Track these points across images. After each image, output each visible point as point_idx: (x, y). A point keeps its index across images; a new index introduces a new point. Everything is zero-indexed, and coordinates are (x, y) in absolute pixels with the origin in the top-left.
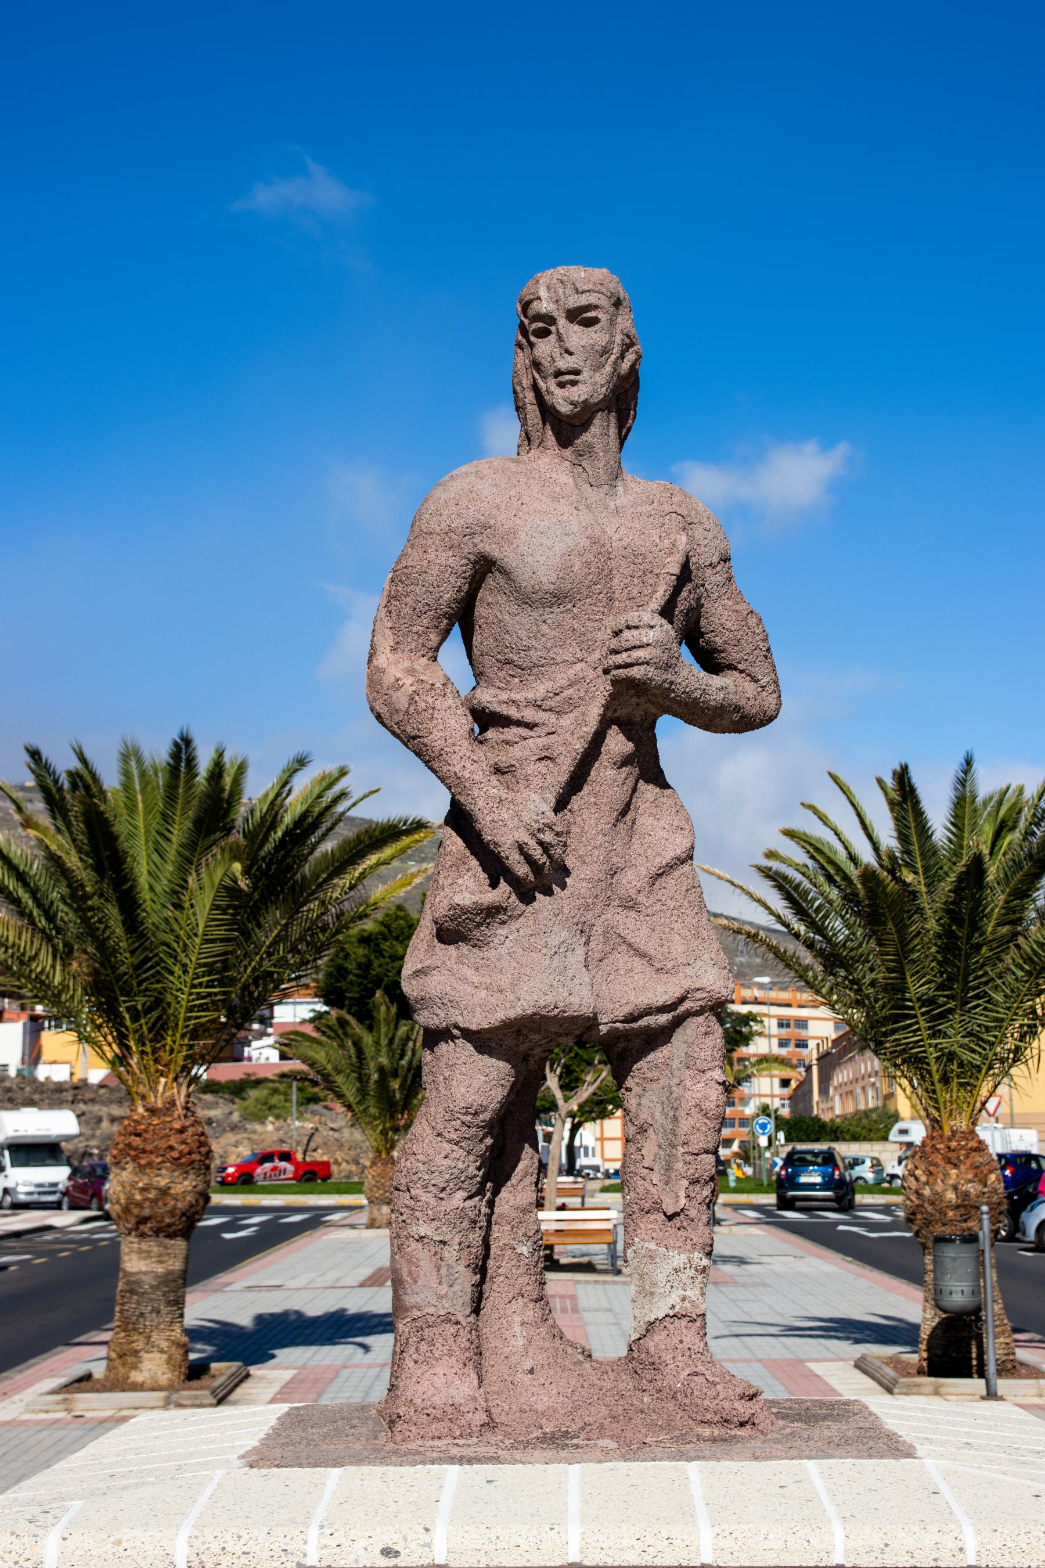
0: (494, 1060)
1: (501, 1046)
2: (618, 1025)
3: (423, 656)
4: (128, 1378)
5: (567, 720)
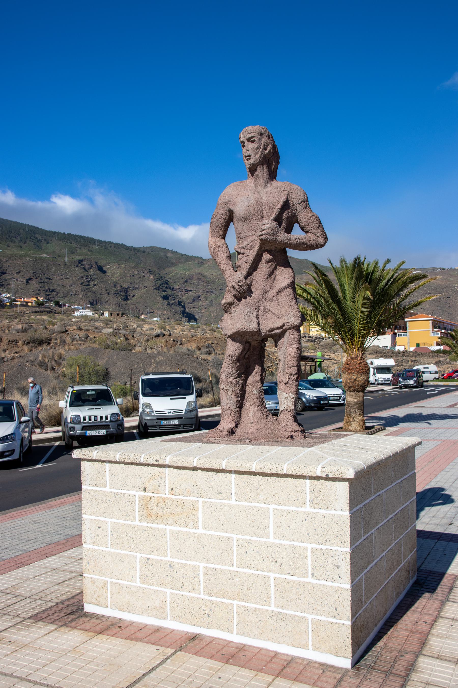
2: (267, 333)
5: (251, 252)
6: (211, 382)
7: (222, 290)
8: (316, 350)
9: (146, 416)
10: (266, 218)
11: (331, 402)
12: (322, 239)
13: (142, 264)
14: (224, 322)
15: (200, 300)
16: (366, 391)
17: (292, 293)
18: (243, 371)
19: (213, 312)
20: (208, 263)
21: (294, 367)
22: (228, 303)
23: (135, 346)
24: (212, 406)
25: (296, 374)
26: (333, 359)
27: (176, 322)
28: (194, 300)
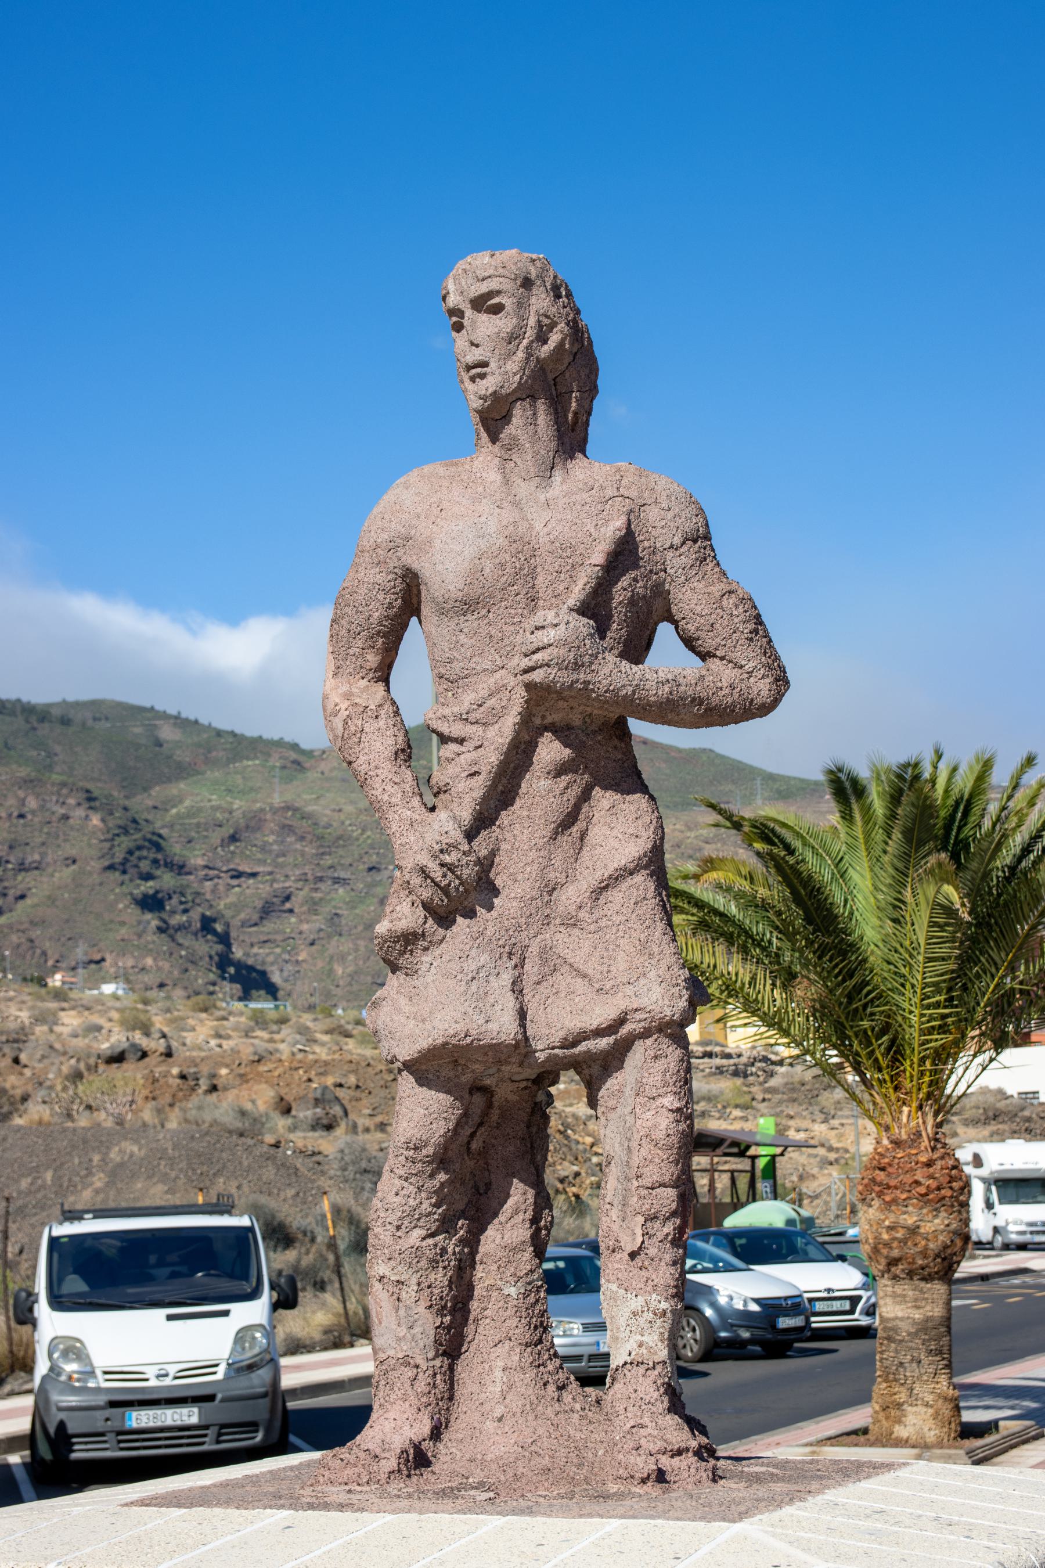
0: (433, 1092)
1: (438, 1077)
2: (557, 1051)
3: (363, 678)
4: (892, 1433)
5: (492, 732)
6: (332, 1245)
7: (379, 870)
8: (752, 1108)
9: (62, 1392)
10: (547, 603)
11: (818, 1322)
12: (767, 680)
13: (58, 769)
14: (386, 1008)
15: (291, 911)
16: (957, 1275)
17: (651, 893)
18: (461, 1206)
19: (342, 958)
20: (323, 766)
21: (663, 1185)
22: (403, 935)
23: (25, 1099)
24: (337, 1345)
25: (674, 1214)
26: (823, 1145)
27: (194, 999)
28: (267, 911)
